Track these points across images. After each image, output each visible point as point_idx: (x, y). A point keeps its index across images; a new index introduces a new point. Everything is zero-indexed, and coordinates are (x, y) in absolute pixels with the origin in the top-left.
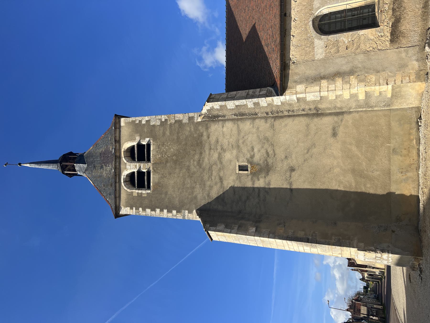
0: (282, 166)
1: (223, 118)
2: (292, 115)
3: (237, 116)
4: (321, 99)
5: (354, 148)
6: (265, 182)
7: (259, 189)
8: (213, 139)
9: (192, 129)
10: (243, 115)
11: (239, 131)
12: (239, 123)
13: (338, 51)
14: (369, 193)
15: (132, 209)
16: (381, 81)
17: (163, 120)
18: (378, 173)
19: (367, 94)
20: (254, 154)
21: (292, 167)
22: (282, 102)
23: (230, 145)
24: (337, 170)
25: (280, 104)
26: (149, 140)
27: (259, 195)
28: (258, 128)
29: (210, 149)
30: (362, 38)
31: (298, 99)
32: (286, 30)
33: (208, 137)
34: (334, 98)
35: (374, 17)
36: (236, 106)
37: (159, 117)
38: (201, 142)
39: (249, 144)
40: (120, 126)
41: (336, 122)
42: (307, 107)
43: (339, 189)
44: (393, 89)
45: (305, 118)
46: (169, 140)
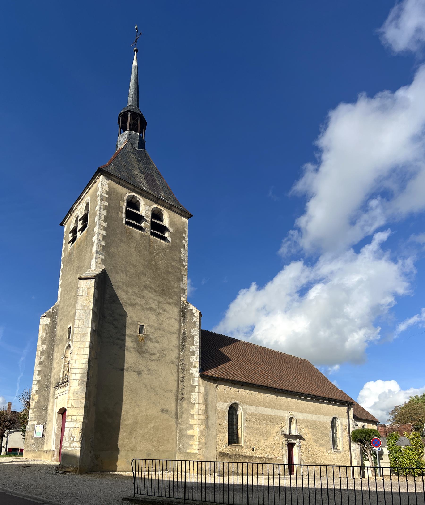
0: (142, 365)
1: (182, 321)
2: (180, 380)
3: (183, 334)
4: (191, 403)
5: (152, 425)
6: (130, 347)
7: (124, 340)
8: (167, 307)
9: (175, 289)
10: (184, 339)
11: (172, 333)
12: (177, 335)
13: (219, 419)
14: (119, 434)
15: (106, 194)
16: (200, 446)
17: (184, 263)
18: (134, 442)
19: (192, 436)
20: (153, 342)
21: (141, 373)
22: (193, 373)
23: (161, 322)
24: (137, 410)
25: (191, 372)
26: (169, 242)
27: (118, 339)
28: (172, 350)
29: (159, 302)
30: (224, 435)
31: (194, 387)
32: (234, 384)
33: (168, 303)
34: (191, 413)
35: (232, 443)
36: (193, 337)
37: (186, 260)
38: (165, 295)
39: (161, 339)
40: (182, 216)
41: (171, 413)
42: (185, 392)
43: (123, 410)
44: (193, 453)
45: (176, 390)
46: (168, 263)
